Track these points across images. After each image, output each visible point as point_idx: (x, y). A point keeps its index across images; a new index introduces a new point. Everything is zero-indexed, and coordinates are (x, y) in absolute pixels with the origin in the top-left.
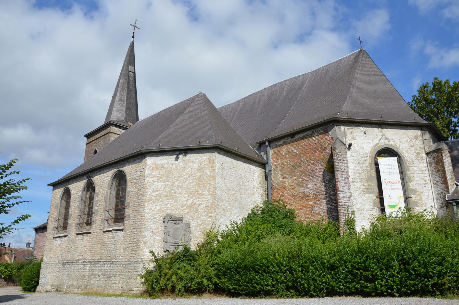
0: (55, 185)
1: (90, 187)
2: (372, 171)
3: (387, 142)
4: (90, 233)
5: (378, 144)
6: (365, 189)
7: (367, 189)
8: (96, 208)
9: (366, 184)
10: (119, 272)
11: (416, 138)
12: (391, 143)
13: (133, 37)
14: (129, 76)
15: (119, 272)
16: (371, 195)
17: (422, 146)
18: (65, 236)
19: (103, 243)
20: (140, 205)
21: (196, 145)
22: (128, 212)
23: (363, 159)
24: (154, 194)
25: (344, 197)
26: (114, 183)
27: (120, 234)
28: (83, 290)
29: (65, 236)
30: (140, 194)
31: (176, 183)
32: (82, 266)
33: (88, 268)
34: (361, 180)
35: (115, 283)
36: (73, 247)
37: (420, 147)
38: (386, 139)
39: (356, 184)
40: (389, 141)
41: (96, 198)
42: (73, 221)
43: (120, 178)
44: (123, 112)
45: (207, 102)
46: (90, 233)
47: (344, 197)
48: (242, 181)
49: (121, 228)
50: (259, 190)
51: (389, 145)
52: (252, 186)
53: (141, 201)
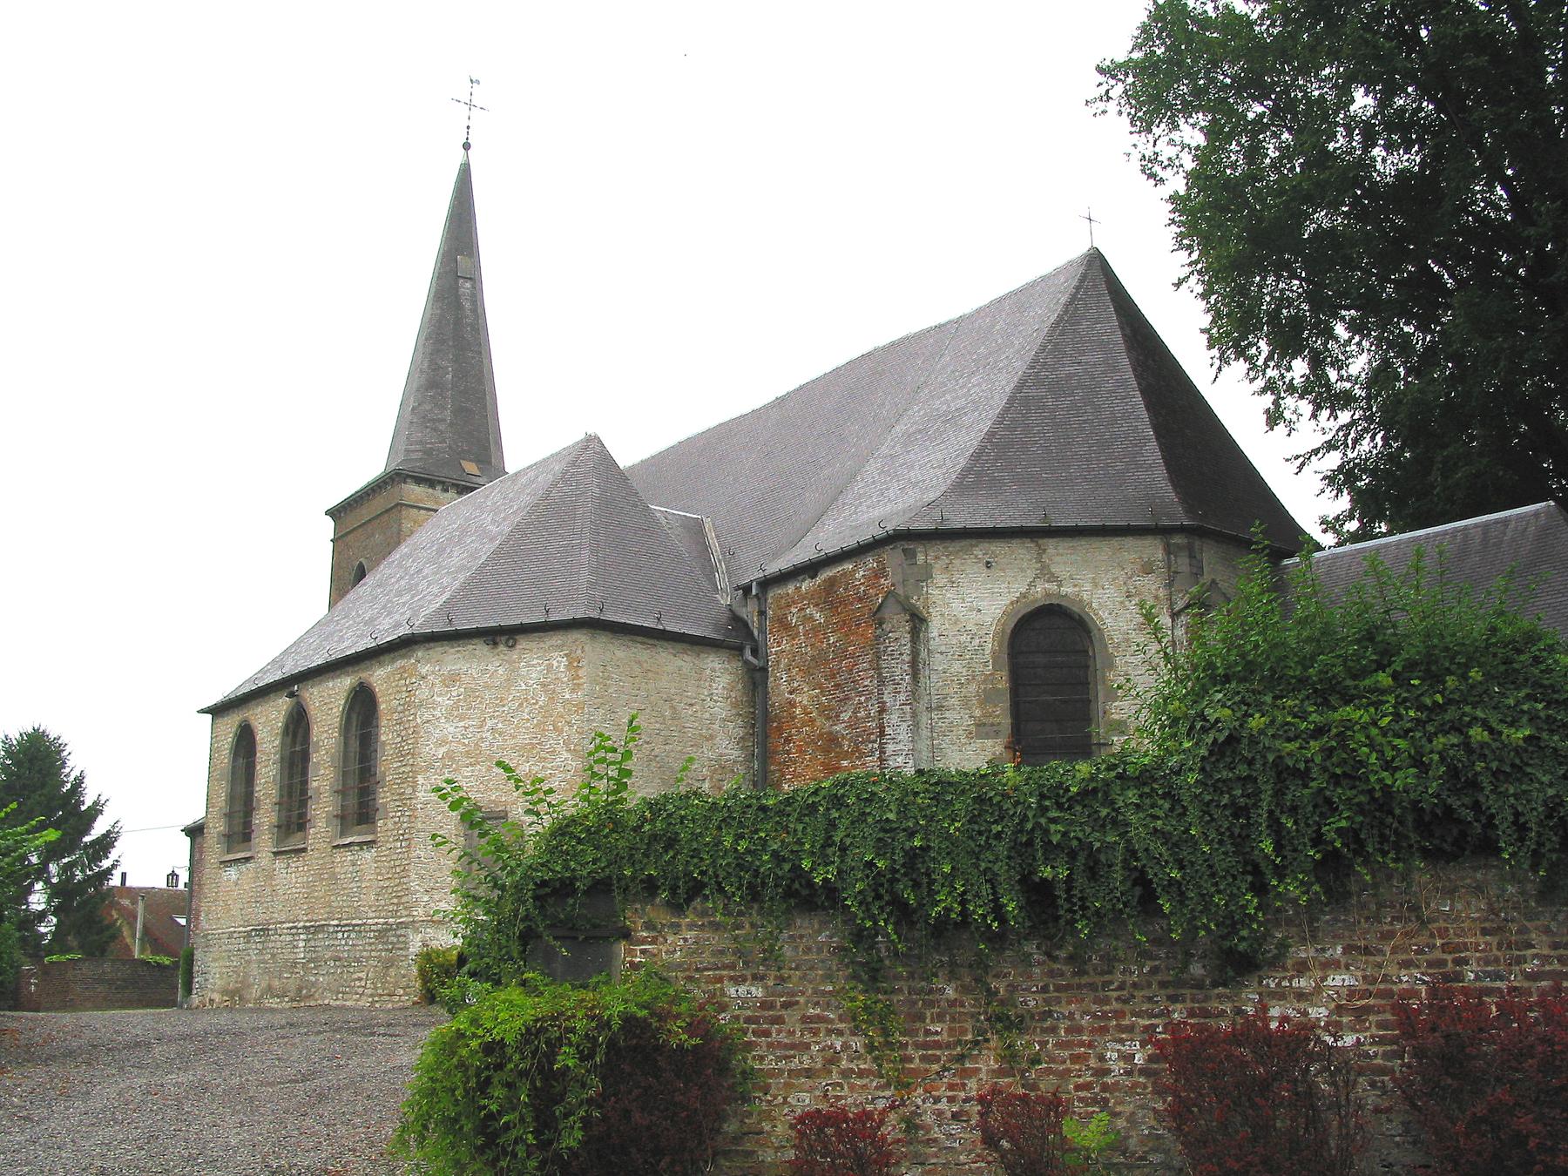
0: (217, 711)
1: (298, 724)
2: (998, 675)
3: (1052, 587)
4: (304, 850)
5: (1024, 596)
6: (973, 728)
7: (977, 725)
8: (315, 784)
9: (977, 713)
10: (1082, 1044)
11: (1147, 569)
12: (1067, 589)
13: (467, 146)
14: (457, 297)
15: (1082, 1044)
16: (989, 742)
17: (1162, 593)
18: (247, 859)
19: (333, 876)
20: (409, 779)
21: (537, 617)
22: (384, 797)
23: (976, 642)
24: (441, 751)
25: (896, 754)
26: (354, 716)
27: (368, 855)
28: (292, 1000)
29: (247, 859)
30: (406, 754)
31: (489, 723)
32: (289, 938)
33: (301, 944)
34: (965, 702)
35: (360, 979)
36: (269, 890)
37: (1156, 597)
38: (1053, 578)
39: (947, 714)
40: (1060, 586)
41: (314, 758)
42: (265, 818)
43: (363, 705)
44: (442, 427)
45: (606, 460)
46: (304, 850)
47: (896, 754)
48: (672, 707)
49: (369, 838)
50: (731, 725)
51: (1059, 595)
52: (707, 715)
53: (408, 769)
